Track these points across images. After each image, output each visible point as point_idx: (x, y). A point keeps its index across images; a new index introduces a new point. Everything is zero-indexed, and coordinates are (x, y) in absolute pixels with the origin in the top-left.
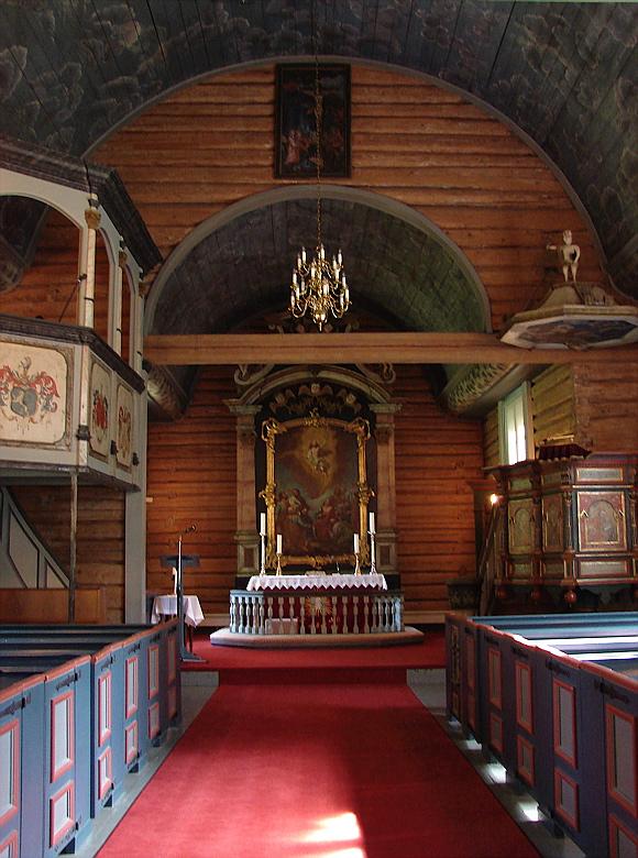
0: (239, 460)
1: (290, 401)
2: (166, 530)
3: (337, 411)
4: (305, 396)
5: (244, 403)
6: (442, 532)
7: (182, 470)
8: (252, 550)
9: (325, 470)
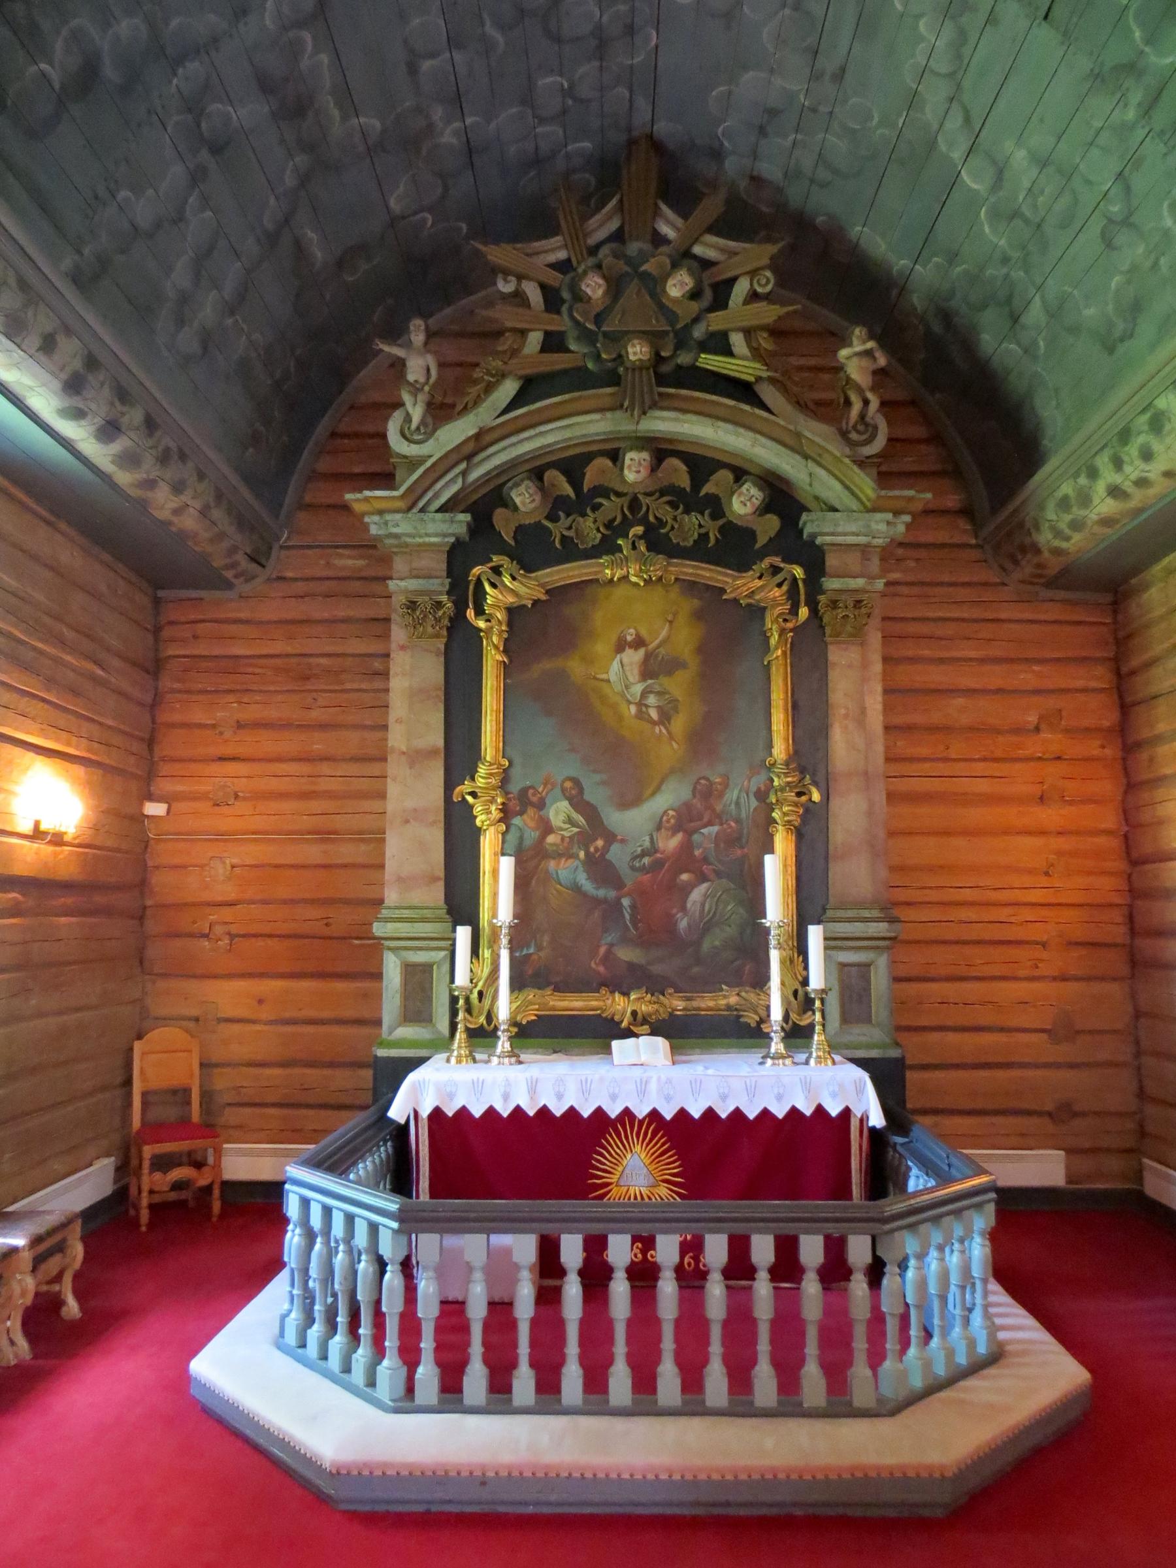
0: (398, 684)
1: (558, 507)
2: (207, 896)
3: (704, 537)
4: (603, 491)
5: (412, 502)
6: (1003, 914)
7: (258, 725)
8: (427, 968)
9: (665, 717)
